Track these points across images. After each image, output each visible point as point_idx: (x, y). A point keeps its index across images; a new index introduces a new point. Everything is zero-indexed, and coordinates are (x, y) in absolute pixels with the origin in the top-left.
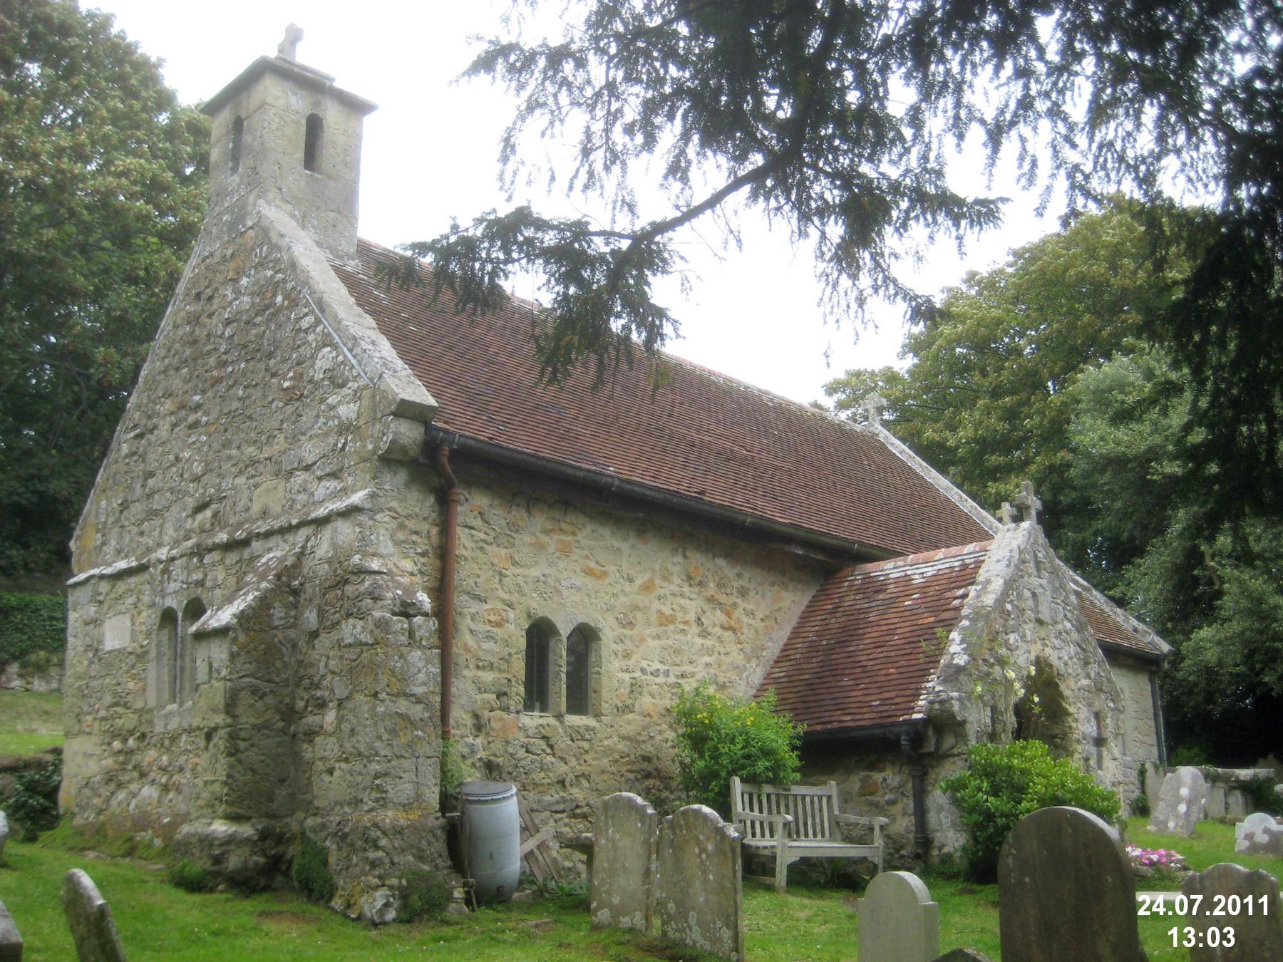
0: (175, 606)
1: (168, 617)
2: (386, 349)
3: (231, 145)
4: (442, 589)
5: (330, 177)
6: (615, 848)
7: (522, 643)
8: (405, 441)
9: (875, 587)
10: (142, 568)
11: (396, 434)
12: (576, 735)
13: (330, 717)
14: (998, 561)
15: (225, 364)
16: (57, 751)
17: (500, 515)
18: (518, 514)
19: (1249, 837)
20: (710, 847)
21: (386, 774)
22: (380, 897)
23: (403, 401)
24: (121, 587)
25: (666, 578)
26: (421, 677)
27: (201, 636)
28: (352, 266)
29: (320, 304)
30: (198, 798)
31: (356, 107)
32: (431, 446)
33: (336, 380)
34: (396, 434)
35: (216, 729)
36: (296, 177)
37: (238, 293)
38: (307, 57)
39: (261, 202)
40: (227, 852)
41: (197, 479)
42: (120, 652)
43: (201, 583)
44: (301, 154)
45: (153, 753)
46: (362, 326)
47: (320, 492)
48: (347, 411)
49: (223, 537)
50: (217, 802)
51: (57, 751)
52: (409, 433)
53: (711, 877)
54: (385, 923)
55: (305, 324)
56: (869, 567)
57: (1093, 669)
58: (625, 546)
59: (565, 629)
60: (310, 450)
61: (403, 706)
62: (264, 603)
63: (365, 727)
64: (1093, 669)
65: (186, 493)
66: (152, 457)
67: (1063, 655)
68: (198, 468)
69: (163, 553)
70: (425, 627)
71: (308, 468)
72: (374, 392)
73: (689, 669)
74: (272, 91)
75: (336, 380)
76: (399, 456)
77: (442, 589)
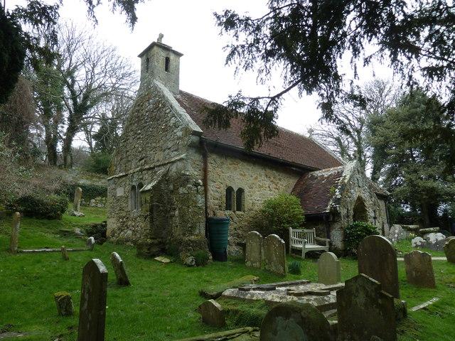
1: (133, 188)
2: (189, 118)
4: (205, 180)
7: (225, 193)
9: (313, 178)
10: (126, 175)
12: (238, 216)
13: (177, 212)
15: (146, 122)
16: (105, 222)
17: (219, 160)
18: (223, 160)
19: (416, 243)
22: (190, 259)
24: (121, 180)
25: (261, 176)
27: (143, 192)
28: (178, 96)
29: (171, 106)
31: (179, 55)
32: (202, 142)
33: (176, 126)
36: (163, 74)
37: (149, 104)
38: (164, 41)
41: (140, 152)
42: (121, 197)
43: (142, 179)
45: (130, 222)
46: (182, 111)
47: (172, 155)
48: (180, 134)
49: (147, 167)
51: (105, 222)
52: (195, 139)
54: (192, 266)
55: (167, 111)
57: (373, 199)
58: (250, 168)
59: (236, 189)
60: (170, 145)
61: (196, 209)
62: (159, 183)
64: (373, 199)
65: (138, 156)
66: (128, 147)
67: (365, 196)
68: (140, 149)
69: (131, 171)
70: (201, 189)
71: (169, 149)
72: (187, 131)
75: (176, 126)
77: (205, 180)
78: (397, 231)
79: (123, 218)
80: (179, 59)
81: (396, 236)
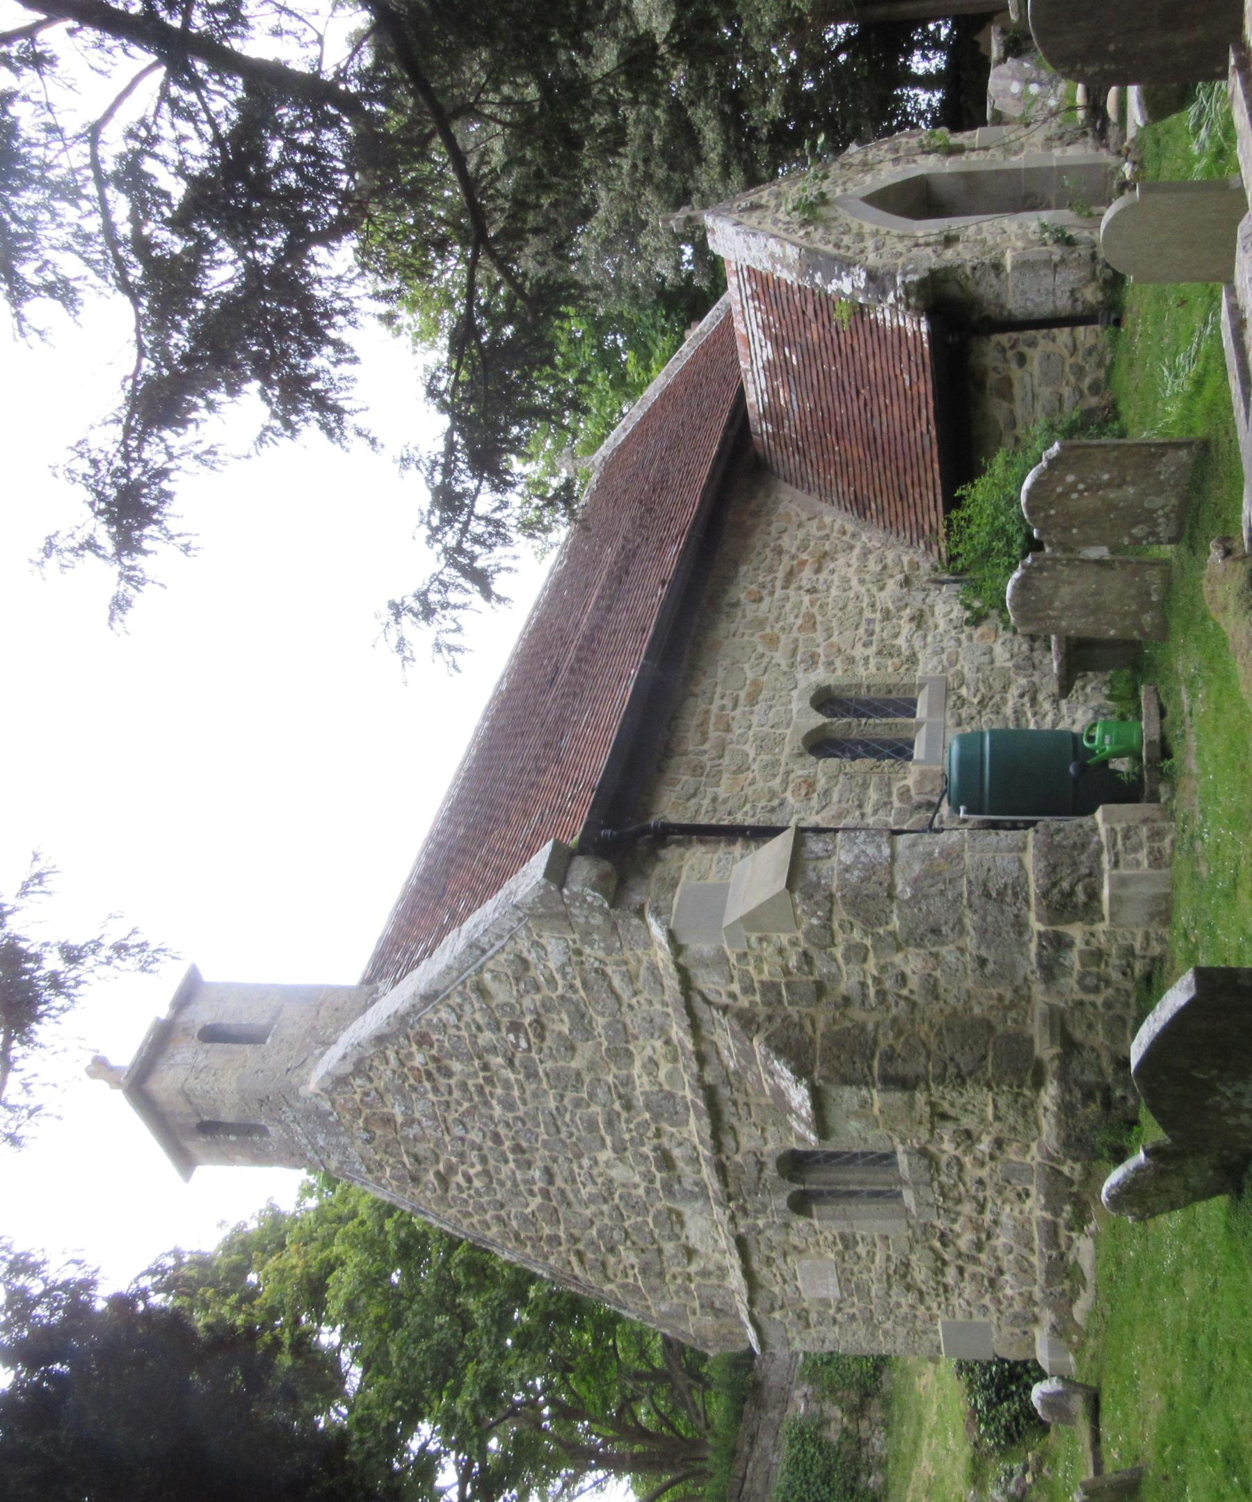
0: (788, 1193)
3: (232, 1138)
5: (274, 1018)
6: (1070, 607)
8: (594, 874)
9: (774, 414)
11: (584, 885)
14: (749, 248)
20: (1070, 478)
21: (985, 885)
23: (546, 875)
24: (763, 1272)
26: (871, 850)
30: (1014, 1129)
34: (584, 885)
35: (932, 1105)
38: (124, 1055)
39: (302, 1091)
40: (1077, 1083)
44: (248, 1048)
46: (454, 945)
50: (1020, 1100)
52: (583, 871)
53: (1106, 477)
56: (752, 415)
59: (818, 720)
63: (929, 912)
73: (866, 601)
74: (165, 1083)
76: (614, 882)
78: (1015, 88)
79: (940, 1266)
80: (210, 985)
81: (1034, 89)
